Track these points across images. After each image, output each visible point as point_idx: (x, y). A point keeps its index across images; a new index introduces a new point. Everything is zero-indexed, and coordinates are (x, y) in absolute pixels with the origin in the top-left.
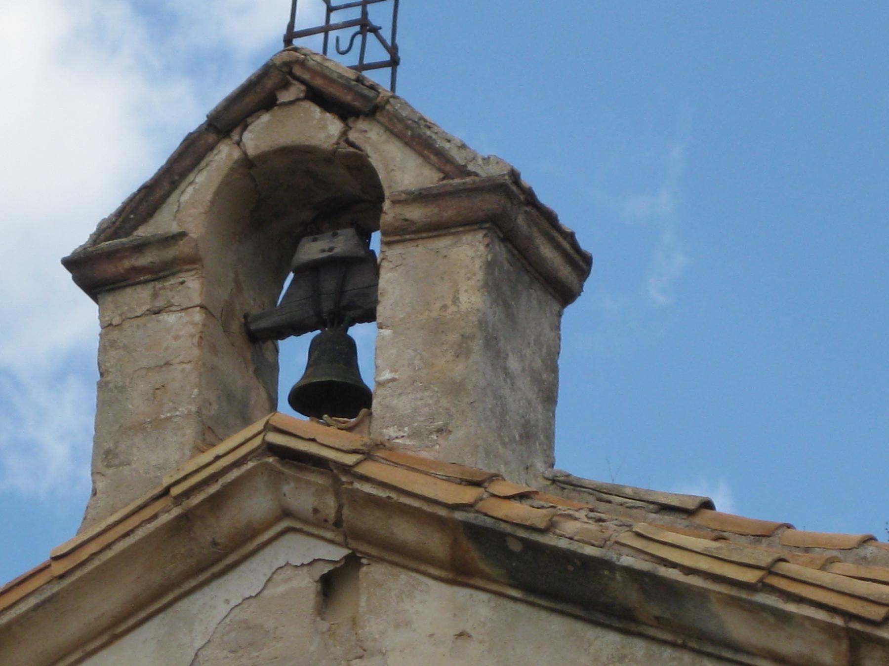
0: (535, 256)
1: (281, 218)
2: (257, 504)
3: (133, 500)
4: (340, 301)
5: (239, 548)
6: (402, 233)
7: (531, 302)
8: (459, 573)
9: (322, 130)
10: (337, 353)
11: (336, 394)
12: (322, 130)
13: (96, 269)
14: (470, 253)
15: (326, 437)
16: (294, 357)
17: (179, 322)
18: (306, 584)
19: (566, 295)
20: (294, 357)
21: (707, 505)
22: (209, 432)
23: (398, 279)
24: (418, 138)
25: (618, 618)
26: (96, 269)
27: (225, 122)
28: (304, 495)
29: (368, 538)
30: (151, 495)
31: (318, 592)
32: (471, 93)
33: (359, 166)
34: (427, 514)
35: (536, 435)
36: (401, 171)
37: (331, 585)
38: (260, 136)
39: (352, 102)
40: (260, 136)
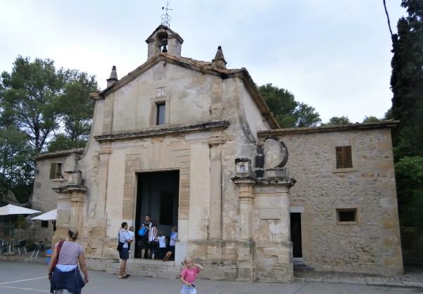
0: (180, 40)
1: (162, 36)
2: (159, 59)
3: (345, 225)
4: (165, 44)
5: (156, 63)
6: (170, 38)
7: (179, 44)
8: (174, 64)
9: (164, 30)
10: (165, 48)
11: (165, 51)
12: (164, 30)
13: (148, 41)
14: (174, 40)
15: (164, 54)
16: (162, 48)
17: (153, 45)
18: (163, 65)
19: (182, 43)
20: (162, 48)
21: (226, 63)
22: (156, 53)
23: (169, 41)
24: (171, 31)
25: (185, 67)
26: (148, 41)
27: (157, 30)
28: (162, 58)
29: (167, 61)
30: (120, 192)
31: (263, 121)
32: (174, 27)
33: (166, 33)
34: (171, 59)
35: (180, 54)
36: (169, 34)
37: (165, 65)
38: (159, 31)
39: (166, 28)
40: (159, 31)
